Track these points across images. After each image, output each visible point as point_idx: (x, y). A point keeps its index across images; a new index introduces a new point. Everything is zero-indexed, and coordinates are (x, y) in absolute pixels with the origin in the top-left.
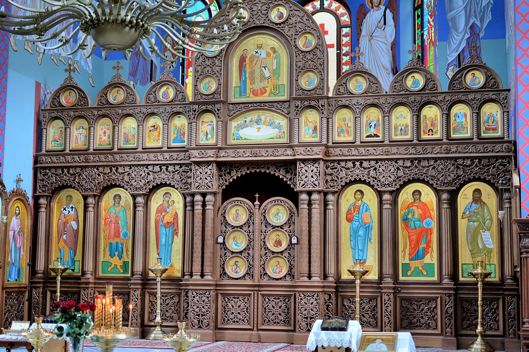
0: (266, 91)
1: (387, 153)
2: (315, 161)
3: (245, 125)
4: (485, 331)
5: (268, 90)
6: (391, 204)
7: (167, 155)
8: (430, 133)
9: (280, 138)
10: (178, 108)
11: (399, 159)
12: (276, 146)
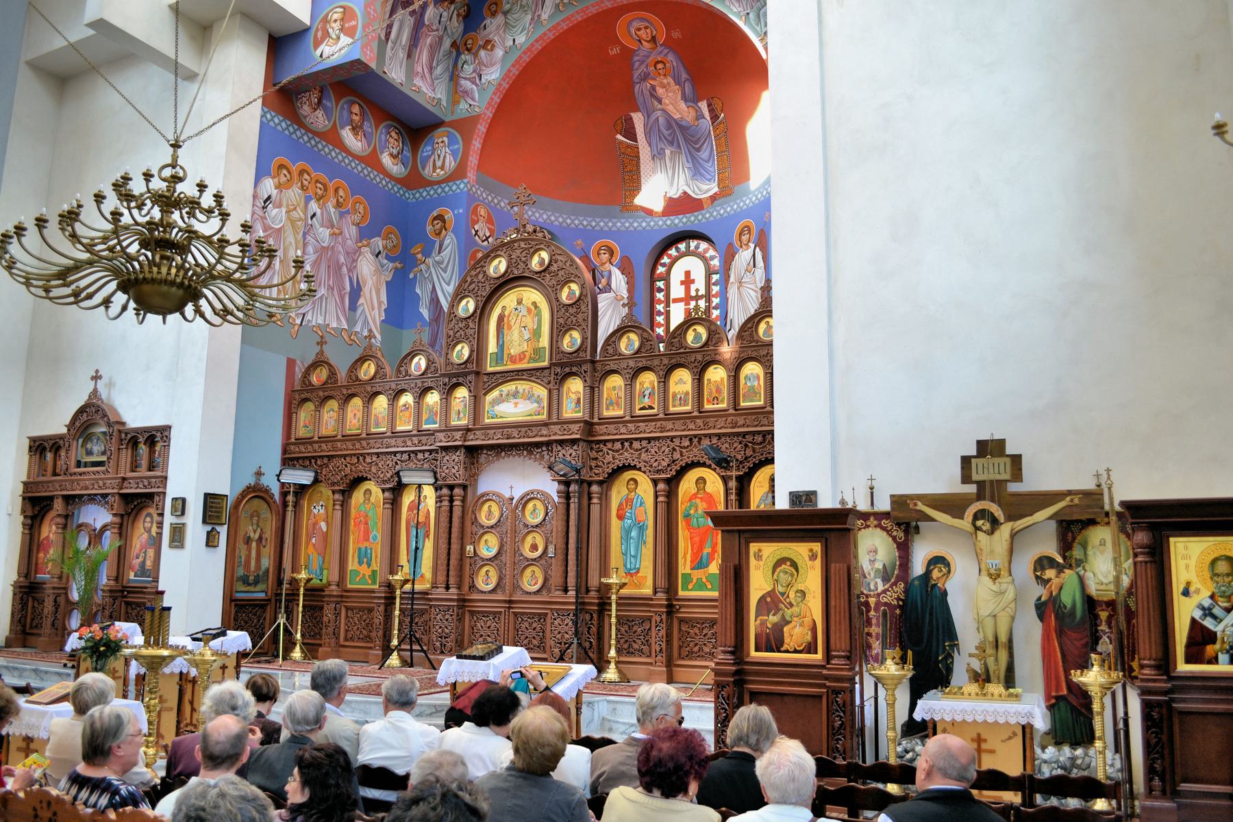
2: (574, 442)
4: (399, 645)
7: (415, 440)
11: (675, 437)
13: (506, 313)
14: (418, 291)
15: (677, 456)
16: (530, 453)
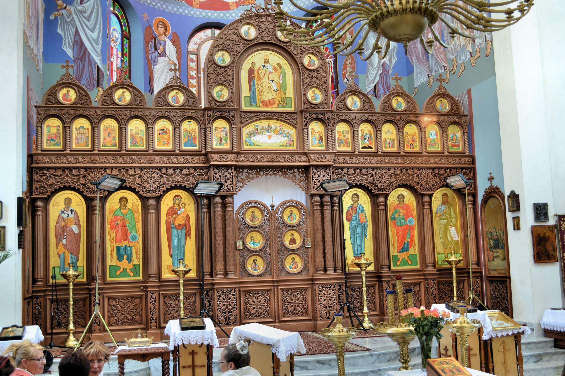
0: (274, 102)
1: (427, 162)
3: (256, 132)
5: (277, 101)
6: (320, 206)
8: (412, 147)
9: (290, 146)
10: (190, 113)
11: (107, 168)
12: (291, 153)
13: (256, 68)
14: (60, 31)
15: (164, 180)
16: (285, 173)
